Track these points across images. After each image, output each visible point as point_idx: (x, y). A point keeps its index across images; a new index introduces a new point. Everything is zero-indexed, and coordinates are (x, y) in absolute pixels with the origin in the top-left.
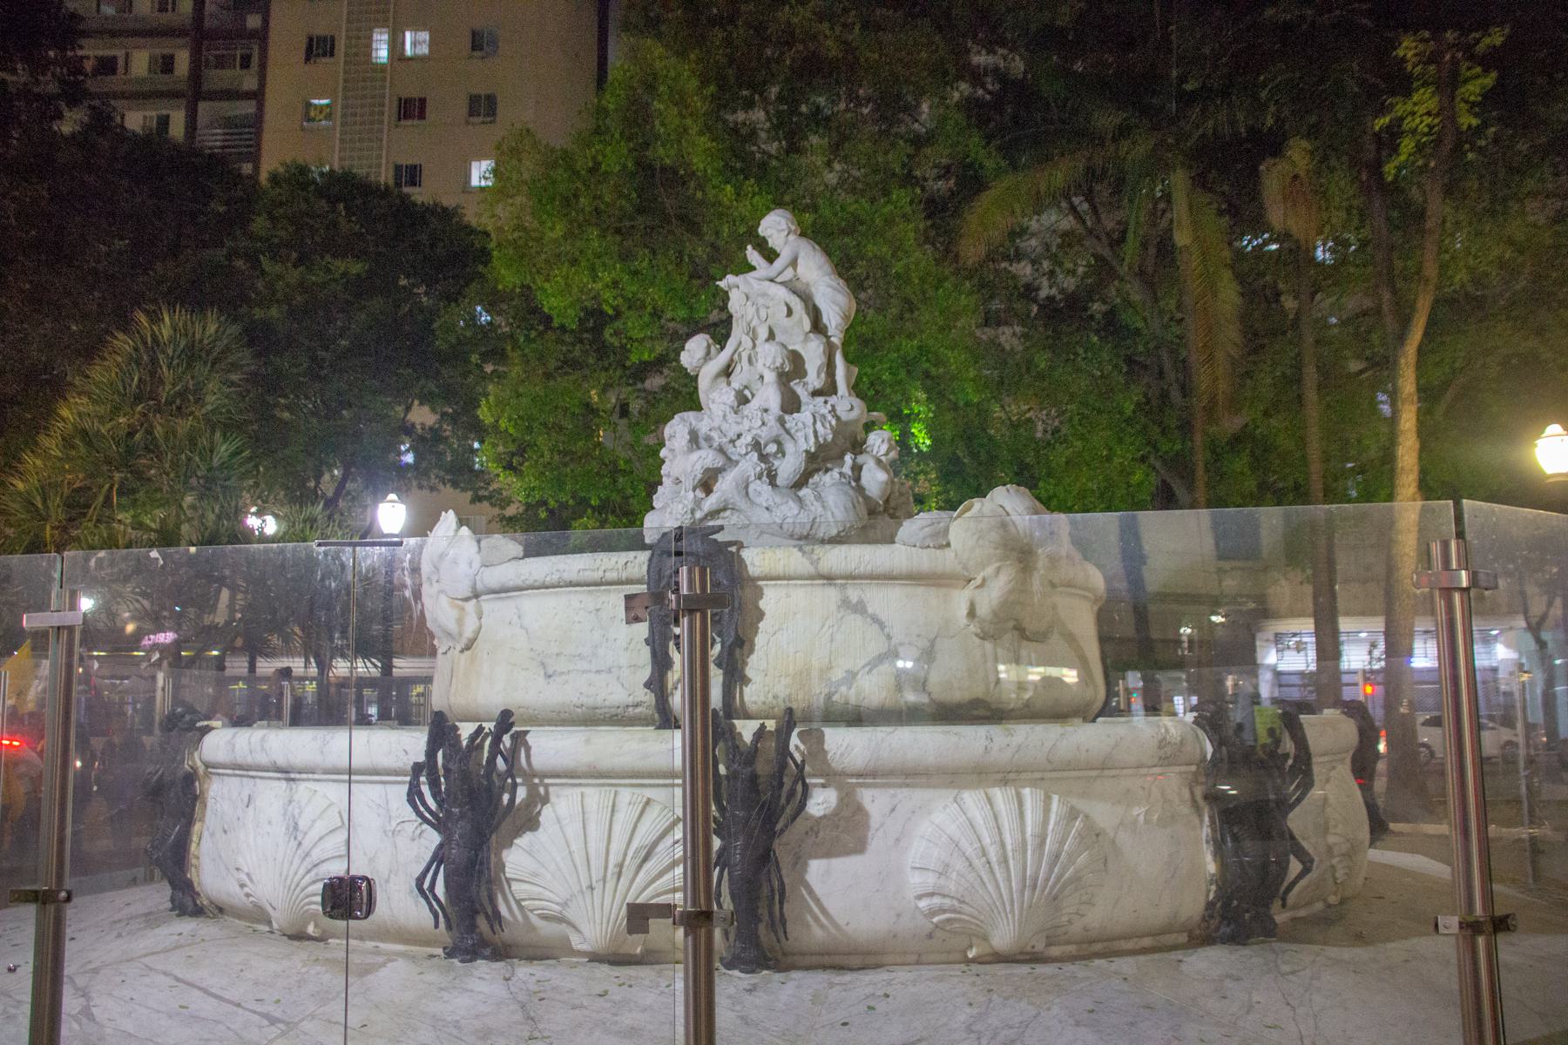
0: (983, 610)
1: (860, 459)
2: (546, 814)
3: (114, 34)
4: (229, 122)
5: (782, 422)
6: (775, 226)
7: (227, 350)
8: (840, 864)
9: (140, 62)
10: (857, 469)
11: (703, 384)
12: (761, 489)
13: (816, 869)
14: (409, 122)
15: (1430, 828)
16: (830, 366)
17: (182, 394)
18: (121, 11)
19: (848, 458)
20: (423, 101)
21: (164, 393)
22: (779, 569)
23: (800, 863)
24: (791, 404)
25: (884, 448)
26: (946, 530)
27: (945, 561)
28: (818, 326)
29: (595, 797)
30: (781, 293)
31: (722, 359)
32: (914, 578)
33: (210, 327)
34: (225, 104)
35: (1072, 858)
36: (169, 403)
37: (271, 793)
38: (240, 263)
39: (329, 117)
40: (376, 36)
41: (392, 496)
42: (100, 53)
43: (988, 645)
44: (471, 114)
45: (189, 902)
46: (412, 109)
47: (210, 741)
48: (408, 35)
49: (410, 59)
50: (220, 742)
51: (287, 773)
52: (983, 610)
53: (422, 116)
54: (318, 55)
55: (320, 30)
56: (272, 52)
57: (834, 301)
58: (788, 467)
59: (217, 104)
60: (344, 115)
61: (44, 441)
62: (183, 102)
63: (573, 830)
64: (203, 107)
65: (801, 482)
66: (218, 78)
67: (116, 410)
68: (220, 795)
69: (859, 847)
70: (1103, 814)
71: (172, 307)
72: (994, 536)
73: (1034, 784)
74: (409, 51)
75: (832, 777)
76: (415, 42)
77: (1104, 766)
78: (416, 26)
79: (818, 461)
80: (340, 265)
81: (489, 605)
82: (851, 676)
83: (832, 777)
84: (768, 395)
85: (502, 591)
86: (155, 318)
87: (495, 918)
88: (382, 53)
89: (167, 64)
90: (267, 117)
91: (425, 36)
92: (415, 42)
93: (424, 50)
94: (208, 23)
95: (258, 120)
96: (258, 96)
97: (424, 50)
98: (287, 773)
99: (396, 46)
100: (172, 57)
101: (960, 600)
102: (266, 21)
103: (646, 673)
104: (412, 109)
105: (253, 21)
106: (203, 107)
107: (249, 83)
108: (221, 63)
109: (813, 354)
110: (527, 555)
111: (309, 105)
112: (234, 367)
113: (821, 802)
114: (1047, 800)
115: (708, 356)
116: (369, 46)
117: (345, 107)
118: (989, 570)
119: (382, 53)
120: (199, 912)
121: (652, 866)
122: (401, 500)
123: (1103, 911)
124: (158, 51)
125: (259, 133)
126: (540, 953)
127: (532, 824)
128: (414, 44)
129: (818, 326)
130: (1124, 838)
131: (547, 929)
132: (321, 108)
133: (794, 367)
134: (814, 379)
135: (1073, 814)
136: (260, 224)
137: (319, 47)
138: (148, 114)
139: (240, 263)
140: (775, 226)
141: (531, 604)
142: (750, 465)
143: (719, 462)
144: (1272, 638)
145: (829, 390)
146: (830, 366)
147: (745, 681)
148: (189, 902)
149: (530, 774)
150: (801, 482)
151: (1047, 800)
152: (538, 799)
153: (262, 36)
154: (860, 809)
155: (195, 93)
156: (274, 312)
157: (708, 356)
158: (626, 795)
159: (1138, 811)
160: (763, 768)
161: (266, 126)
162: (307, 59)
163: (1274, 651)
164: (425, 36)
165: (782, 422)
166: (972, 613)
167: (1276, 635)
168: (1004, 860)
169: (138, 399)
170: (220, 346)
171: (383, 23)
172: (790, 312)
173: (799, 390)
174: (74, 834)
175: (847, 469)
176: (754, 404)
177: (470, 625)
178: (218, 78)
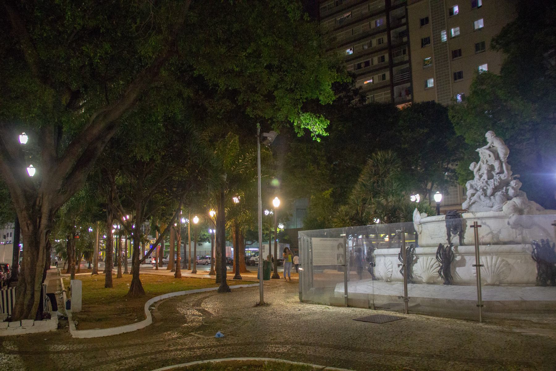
0: (511, 223)
1: (508, 188)
2: (418, 261)
3: (368, 54)
4: (402, 71)
5: (487, 182)
7: (394, 160)
9: (376, 60)
10: (507, 190)
11: (475, 173)
12: (482, 197)
14: (457, 58)
16: (501, 166)
18: (369, 47)
19: (504, 188)
20: (460, 50)
22: (468, 217)
23: (455, 268)
24: (490, 177)
25: (514, 184)
26: (502, 208)
27: (502, 213)
29: (425, 258)
31: (478, 167)
32: (495, 217)
33: (390, 154)
35: (502, 268)
36: (382, 175)
37: (382, 259)
38: (397, 134)
39: (431, 63)
40: (442, 33)
42: (365, 61)
45: (374, 278)
46: (457, 54)
47: (375, 251)
49: (454, 37)
50: (377, 251)
52: (511, 223)
53: (460, 55)
54: (425, 44)
55: (424, 36)
56: (412, 48)
57: (501, 150)
58: (489, 192)
61: (356, 186)
62: (388, 69)
67: (370, 178)
68: (377, 260)
69: (464, 265)
70: (511, 261)
73: (496, 255)
78: (454, 27)
79: (496, 189)
80: (422, 131)
81: (423, 226)
84: (485, 177)
85: (424, 223)
86: (376, 154)
87: (412, 277)
88: (445, 38)
89: (383, 59)
93: (458, 33)
94: (393, 43)
95: (410, 70)
96: (409, 61)
97: (458, 33)
98: (384, 256)
99: (449, 34)
100: (384, 56)
101: (506, 220)
102: (408, 38)
103: (447, 238)
104: (457, 54)
106: (394, 69)
107: (406, 58)
109: (496, 165)
110: (428, 216)
111: (425, 61)
113: (458, 258)
115: (475, 167)
116: (440, 37)
118: (511, 215)
119: (445, 38)
120: (376, 280)
121: (433, 268)
122: (440, 193)
124: (379, 56)
125: (411, 73)
126: (420, 282)
128: (455, 32)
129: (497, 157)
132: (428, 61)
133: (492, 168)
134: (497, 170)
135: (503, 260)
136: (401, 122)
137: (425, 42)
139: (397, 134)
140: (489, 135)
141: (430, 226)
142: (480, 192)
143: (474, 192)
145: (502, 172)
146: (501, 166)
148: (374, 278)
149: (416, 255)
150: (493, 194)
153: (408, 43)
154: (465, 259)
155: (391, 65)
156: (406, 146)
158: (429, 257)
160: (447, 253)
162: (422, 47)
165: (487, 182)
166: (509, 224)
168: (488, 268)
170: (392, 159)
171: (443, 29)
172: (490, 156)
174: (256, 165)
175: (504, 191)
176: (483, 178)
177: (420, 229)
178: (396, 60)
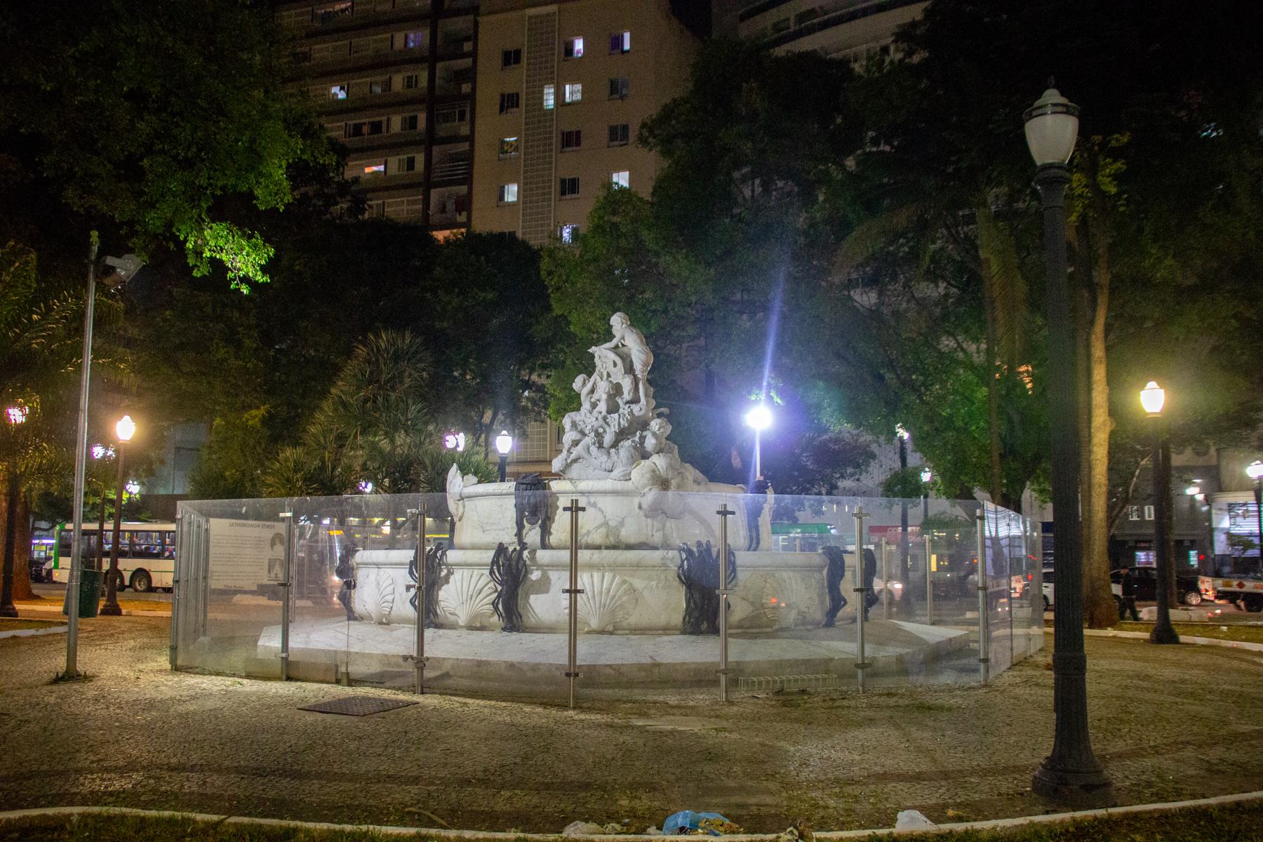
3: (380, 106)
6: (617, 321)
7: (416, 352)
8: (541, 597)
9: (396, 123)
10: (643, 438)
13: (532, 598)
15: (969, 615)
17: (394, 377)
20: (578, 133)
21: (384, 377)
23: (527, 596)
24: (612, 408)
27: (629, 485)
28: (630, 369)
29: (467, 572)
30: (612, 356)
31: (589, 386)
32: (615, 493)
33: (407, 340)
34: (448, 146)
35: (620, 598)
37: (373, 572)
39: (517, 149)
40: (546, 91)
41: (504, 432)
43: (649, 520)
44: (612, 140)
46: (571, 139)
48: (567, 87)
49: (569, 104)
51: (378, 565)
52: (645, 506)
53: (578, 144)
55: (508, 90)
58: (608, 439)
59: (443, 146)
60: (526, 148)
63: (459, 584)
64: (435, 149)
65: (615, 445)
66: (443, 130)
67: (359, 388)
69: (547, 591)
70: (638, 583)
71: (386, 329)
72: (648, 476)
74: (568, 100)
75: (540, 567)
76: (572, 92)
77: (638, 566)
79: (622, 435)
82: (589, 532)
83: (540, 567)
86: (378, 336)
87: (436, 614)
88: (550, 101)
89: (412, 123)
90: (477, 153)
91: (579, 87)
92: (572, 92)
93: (578, 97)
94: (438, 92)
96: (470, 139)
97: (578, 97)
98: (378, 565)
99: (559, 95)
101: (636, 501)
102: (474, 89)
105: (466, 88)
106: (435, 149)
107: (465, 130)
108: (447, 118)
109: (627, 383)
110: (479, 482)
111: (503, 142)
112: (420, 361)
113: (535, 575)
114: (614, 577)
115: (584, 384)
117: (527, 141)
119: (550, 101)
120: (355, 619)
123: (636, 618)
124: (407, 115)
125: (470, 166)
127: (447, 582)
128: (572, 93)
129: (630, 369)
130: (646, 593)
131: (452, 618)
132: (510, 144)
134: (627, 396)
135: (624, 582)
136: (438, 271)
137: (509, 102)
138: (402, 157)
140: (617, 321)
144: (1225, 507)
145: (635, 400)
146: (636, 388)
147: (550, 534)
149: (447, 565)
150: (615, 445)
151: (614, 577)
152: (450, 573)
153: (471, 97)
157: (584, 384)
159: (654, 583)
161: (476, 160)
162: (501, 110)
163: (1227, 518)
164: (579, 87)
165: (605, 419)
166: (640, 507)
167: (1230, 505)
169: (370, 382)
170: (413, 350)
171: (549, 81)
172: (615, 365)
173: (620, 401)
175: (637, 439)
176: (598, 409)
178: (443, 130)
